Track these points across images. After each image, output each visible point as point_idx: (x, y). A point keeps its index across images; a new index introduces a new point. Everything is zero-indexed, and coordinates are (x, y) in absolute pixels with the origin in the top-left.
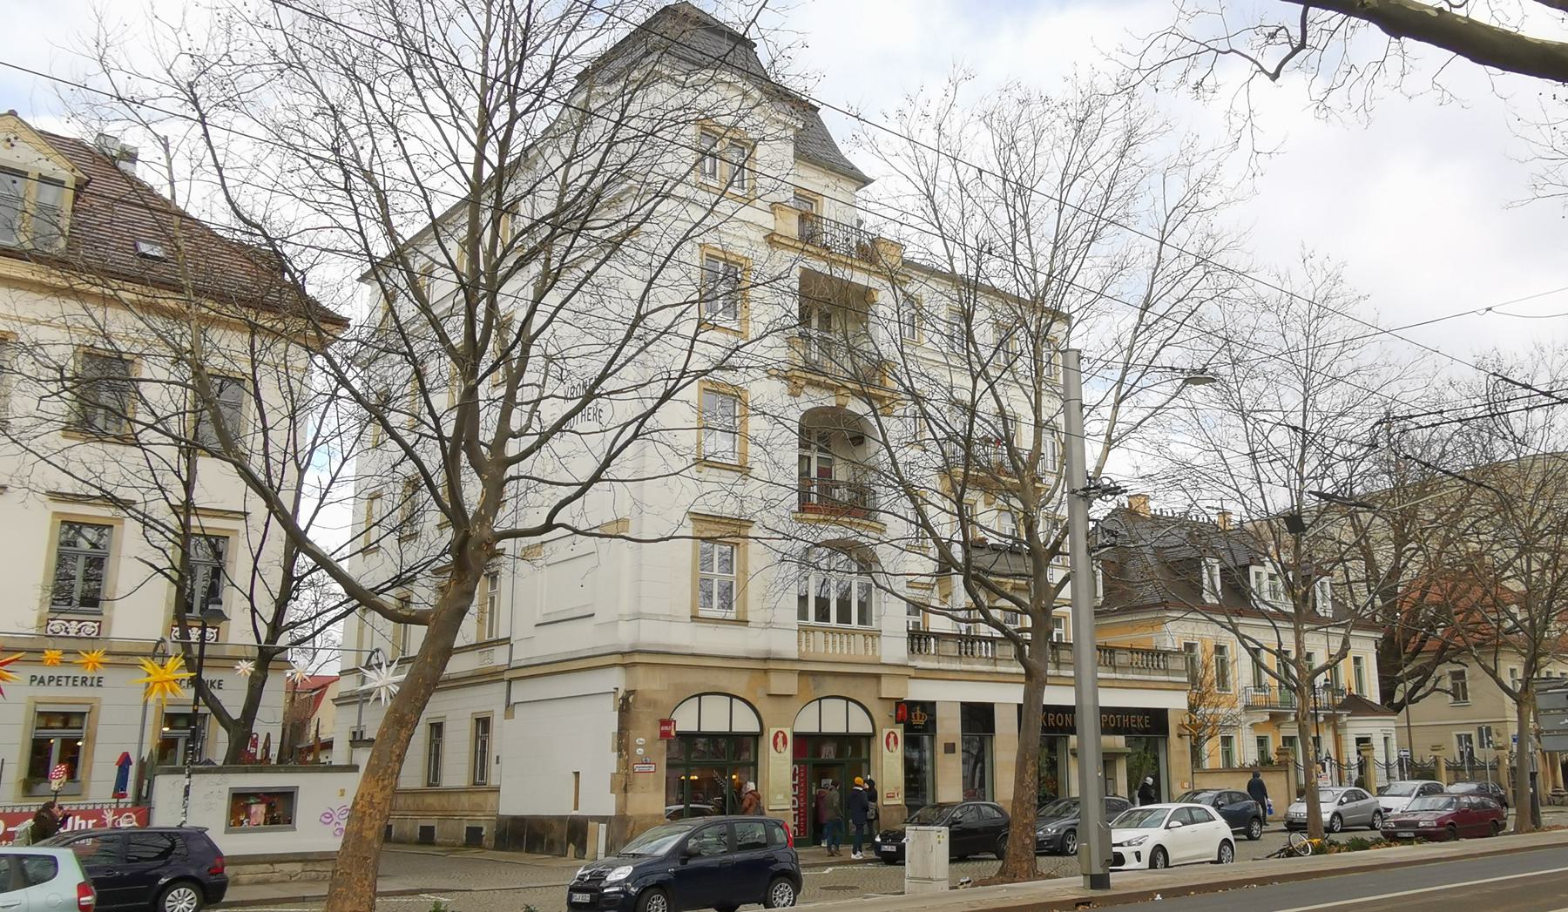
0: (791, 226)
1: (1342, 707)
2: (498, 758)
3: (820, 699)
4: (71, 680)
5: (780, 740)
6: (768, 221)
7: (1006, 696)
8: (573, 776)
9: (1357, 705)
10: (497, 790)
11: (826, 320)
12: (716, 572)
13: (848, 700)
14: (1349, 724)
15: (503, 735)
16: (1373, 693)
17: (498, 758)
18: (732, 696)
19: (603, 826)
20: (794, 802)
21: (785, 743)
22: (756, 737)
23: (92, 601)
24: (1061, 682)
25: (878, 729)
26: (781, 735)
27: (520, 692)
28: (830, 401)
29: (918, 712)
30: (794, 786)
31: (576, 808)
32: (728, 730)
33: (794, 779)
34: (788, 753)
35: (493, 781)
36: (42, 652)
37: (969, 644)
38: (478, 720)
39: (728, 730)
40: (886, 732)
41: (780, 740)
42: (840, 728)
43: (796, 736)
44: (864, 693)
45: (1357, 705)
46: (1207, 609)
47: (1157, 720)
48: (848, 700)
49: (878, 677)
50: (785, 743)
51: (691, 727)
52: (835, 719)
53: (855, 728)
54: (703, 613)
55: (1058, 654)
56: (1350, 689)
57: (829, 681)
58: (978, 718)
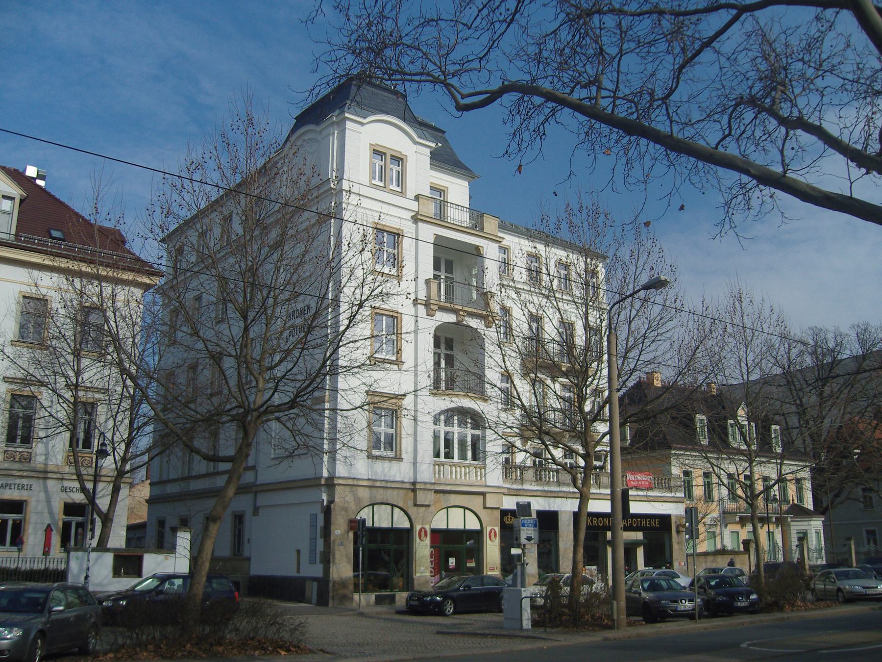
0: (430, 209)
1: (787, 512)
2: (249, 540)
3: (447, 508)
4: (16, 486)
5: (492, 534)
6: (414, 206)
7: (567, 506)
8: (295, 554)
9: (799, 511)
10: (248, 559)
11: (449, 268)
12: (383, 428)
13: (465, 508)
14: (792, 523)
15: (253, 527)
16: (809, 504)
17: (249, 540)
18: (393, 506)
19: (315, 584)
20: (431, 572)
21: (495, 536)
22: (409, 532)
23: (27, 440)
24: (600, 497)
25: (484, 526)
26: (423, 530)
27: (263, 499)
28: (451, 318)
29: (509, 516)
30: (431, 562)
31: (298, 571)
32: (446, 527)
33: (431, 558)
34: (427, 541)
35: (246, 553)
36: (13, 543)
37: (547, 473)
38: (236, 516)
39: (390, 526)
40: (489, 529)
41: (492, 534)
42: (385, 524)
43: (434, 532)
44: (476, 503)
45: (799, 511)
46: (702, 449)
47: (665, 520)
48: (465, 508)
49: (483, 494)
50: (495, 536)
51: (443, 526)
52: (457, 520)
53: (398, 525)
54: (376, 452)
55: (599, 479)
56: (793, 500)
57: (453, 496)
58: (549, 521)
